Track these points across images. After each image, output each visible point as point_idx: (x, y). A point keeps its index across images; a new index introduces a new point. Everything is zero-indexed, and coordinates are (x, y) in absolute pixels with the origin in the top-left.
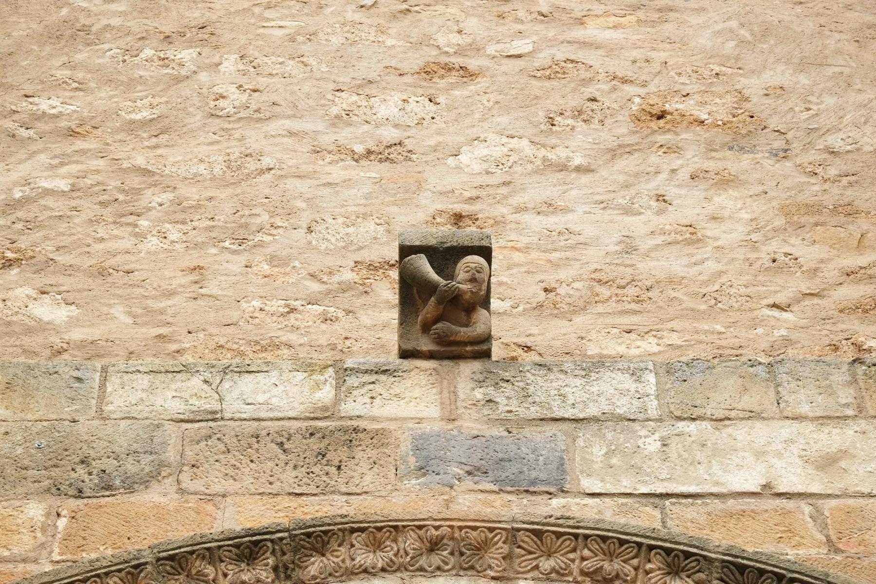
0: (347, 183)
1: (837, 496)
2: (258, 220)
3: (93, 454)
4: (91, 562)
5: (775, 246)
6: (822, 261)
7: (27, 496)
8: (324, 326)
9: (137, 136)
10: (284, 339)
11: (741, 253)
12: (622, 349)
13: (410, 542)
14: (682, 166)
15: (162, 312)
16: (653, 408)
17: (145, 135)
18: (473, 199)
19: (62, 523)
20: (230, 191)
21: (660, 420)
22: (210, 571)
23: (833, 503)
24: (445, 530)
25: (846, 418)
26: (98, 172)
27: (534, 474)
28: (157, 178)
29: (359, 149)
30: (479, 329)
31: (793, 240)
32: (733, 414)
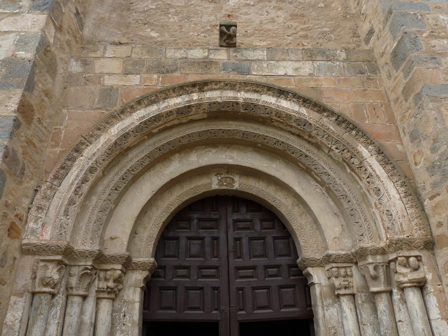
0: (208, 8)
2: (191, 15)
3: (165, 65)
4: (167, 87)
5: (289, 23)
6: (297, 26)
7: (154, 73)
8: (205, 38)
11: (282, 24)
12: (259, 44)
13: (222, 84)
14: (272, 5)
15: (175, 35)
16: (266, 59)
18: (232, 12)
19: (160, 79)
20: (186, 9)
21: (267, 60)
22: (187, 89)
23: (297, 77)
24: (228, 82)
25: (301, 60)
26: (160, 4)
27: (244, 71)
30: (234, 42)
31: (292, 22)
32: (280, 59)
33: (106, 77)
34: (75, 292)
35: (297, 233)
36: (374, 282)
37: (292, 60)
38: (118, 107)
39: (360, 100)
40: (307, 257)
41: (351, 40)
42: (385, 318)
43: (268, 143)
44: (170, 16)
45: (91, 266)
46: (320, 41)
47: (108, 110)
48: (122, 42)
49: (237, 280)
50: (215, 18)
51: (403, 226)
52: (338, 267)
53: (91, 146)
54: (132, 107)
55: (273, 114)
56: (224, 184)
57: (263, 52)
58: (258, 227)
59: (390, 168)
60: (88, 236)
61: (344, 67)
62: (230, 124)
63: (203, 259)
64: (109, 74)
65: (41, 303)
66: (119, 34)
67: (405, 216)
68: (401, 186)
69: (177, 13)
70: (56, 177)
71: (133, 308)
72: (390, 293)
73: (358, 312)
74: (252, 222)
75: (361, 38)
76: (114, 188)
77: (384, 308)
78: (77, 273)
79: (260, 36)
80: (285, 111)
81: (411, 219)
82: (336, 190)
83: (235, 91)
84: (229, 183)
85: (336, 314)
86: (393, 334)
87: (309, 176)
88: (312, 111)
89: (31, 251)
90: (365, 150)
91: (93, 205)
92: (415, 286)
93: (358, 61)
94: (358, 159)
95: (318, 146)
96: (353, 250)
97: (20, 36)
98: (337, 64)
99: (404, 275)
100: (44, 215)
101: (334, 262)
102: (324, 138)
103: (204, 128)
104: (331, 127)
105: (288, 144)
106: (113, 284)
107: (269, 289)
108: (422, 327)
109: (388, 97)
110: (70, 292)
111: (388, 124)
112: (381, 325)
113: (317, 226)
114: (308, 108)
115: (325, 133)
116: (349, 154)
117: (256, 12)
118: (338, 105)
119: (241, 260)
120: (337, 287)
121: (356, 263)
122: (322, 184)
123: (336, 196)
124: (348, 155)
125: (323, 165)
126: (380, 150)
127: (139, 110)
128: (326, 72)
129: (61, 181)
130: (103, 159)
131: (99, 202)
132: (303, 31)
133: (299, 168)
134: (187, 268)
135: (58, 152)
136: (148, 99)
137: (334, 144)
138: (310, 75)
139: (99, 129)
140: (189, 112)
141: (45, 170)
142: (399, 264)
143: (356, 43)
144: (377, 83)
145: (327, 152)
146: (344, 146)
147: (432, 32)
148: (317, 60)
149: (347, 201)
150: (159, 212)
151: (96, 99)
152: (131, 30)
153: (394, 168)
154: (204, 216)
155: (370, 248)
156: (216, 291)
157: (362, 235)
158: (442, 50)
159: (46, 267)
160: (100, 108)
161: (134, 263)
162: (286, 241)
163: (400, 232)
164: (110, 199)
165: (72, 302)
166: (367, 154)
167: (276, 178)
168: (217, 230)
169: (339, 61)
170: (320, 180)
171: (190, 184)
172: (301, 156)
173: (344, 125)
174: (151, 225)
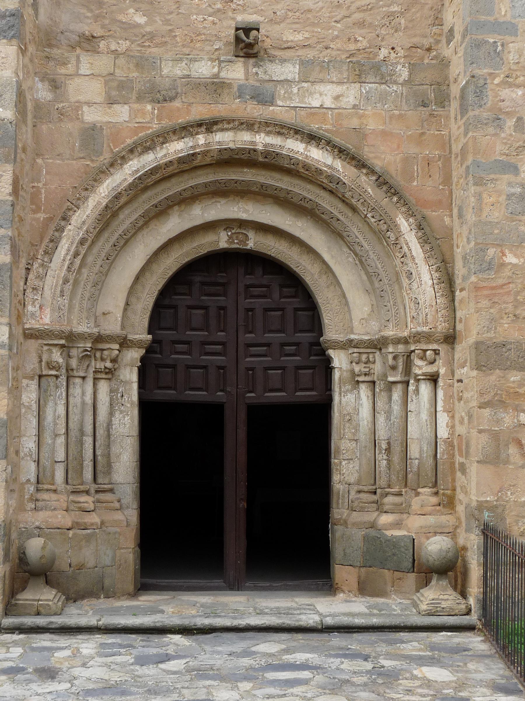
1: (338, 109)
6: (352, 3)
12: (292, 38)
13: (237, 123)
15: (169, 20)
16: (297, 79)
19: (156, 111)
22: (191, 129)
23: (336, 111)
24: (245, 121)
25: (344, 83)
30: (255, 51)
32: (317, 80)
33: (85, 108)
34: (75, 373)
35: (322, 308)
36: (392, 371)
37: (333, 82)
38: (106, 157)
39: (413, 150)
42: (396, 408)
43: (292, 198)
45: (91, 347)
47: (92, 161)
48: (95, 35)
49: (247, 359)
53: (79, 212)
54: (123, 158)
55: (300, 166)
56: (236, 241)
57: (295, 67)
58: (276, 295)
61: (402, 94)
62: (245, 172)
63: (206, 333)
64: (89, 104)
65: (49, 386)
66: (87, 17)
68: (436, 271)
70: (46, 253)
71: (131, 389)
72: (407, 383)
76: (105, 258)
77: (397, 398)
79: (294, 23)
80: (315, 164)
83: (253, 133)
84: (242, 241)
88: (348, 166)
90: (405, 222)
91: (84, 279)
92: (429, 379)
93: (423, 85)
94: (394, 234)
95: (354, 209)
98: (393, 90)
99: (420, 368)
100: (40, 296)
101: (355, 347)
102: (360, 203)
104: (369, 190)
107: (284, 369)
108: (426, 418)
109: (450, 146)
110: (71, 373)
111: (441, 187)
114: (344, 160)
116: (386, 226)
118: (383, 156)
119: (253, 335)
121: (380, 349)
124: (384, 227)
125: (357, 233)
127: (132, 160)
128: (375, 103)
130: (93, 227)
131: (90, 276)
132: (360, 11)
135: (42, 219)
136: (142, 145)
137: (370, 212)
138: (355, 107)
139: (86, 189)
140: (193, 160)
141: (30, 242)
143: (435, 37)
145: (363, 217)
146: (381, 215)
147: (507, 77)
148: (367, 81)
149: (378, 279)
150: (154, 278)
152: (105, 11)
156: (222, 371)
158: (510, 107)
159: (50, 352)
160: (83, 158)
161: (129, 340)
162: (310, 313)
163: (423, 323)
164: (102, 271)
165: (74, 383)
172: (332, 218)
173: (385, 188)
174: (146, 294)
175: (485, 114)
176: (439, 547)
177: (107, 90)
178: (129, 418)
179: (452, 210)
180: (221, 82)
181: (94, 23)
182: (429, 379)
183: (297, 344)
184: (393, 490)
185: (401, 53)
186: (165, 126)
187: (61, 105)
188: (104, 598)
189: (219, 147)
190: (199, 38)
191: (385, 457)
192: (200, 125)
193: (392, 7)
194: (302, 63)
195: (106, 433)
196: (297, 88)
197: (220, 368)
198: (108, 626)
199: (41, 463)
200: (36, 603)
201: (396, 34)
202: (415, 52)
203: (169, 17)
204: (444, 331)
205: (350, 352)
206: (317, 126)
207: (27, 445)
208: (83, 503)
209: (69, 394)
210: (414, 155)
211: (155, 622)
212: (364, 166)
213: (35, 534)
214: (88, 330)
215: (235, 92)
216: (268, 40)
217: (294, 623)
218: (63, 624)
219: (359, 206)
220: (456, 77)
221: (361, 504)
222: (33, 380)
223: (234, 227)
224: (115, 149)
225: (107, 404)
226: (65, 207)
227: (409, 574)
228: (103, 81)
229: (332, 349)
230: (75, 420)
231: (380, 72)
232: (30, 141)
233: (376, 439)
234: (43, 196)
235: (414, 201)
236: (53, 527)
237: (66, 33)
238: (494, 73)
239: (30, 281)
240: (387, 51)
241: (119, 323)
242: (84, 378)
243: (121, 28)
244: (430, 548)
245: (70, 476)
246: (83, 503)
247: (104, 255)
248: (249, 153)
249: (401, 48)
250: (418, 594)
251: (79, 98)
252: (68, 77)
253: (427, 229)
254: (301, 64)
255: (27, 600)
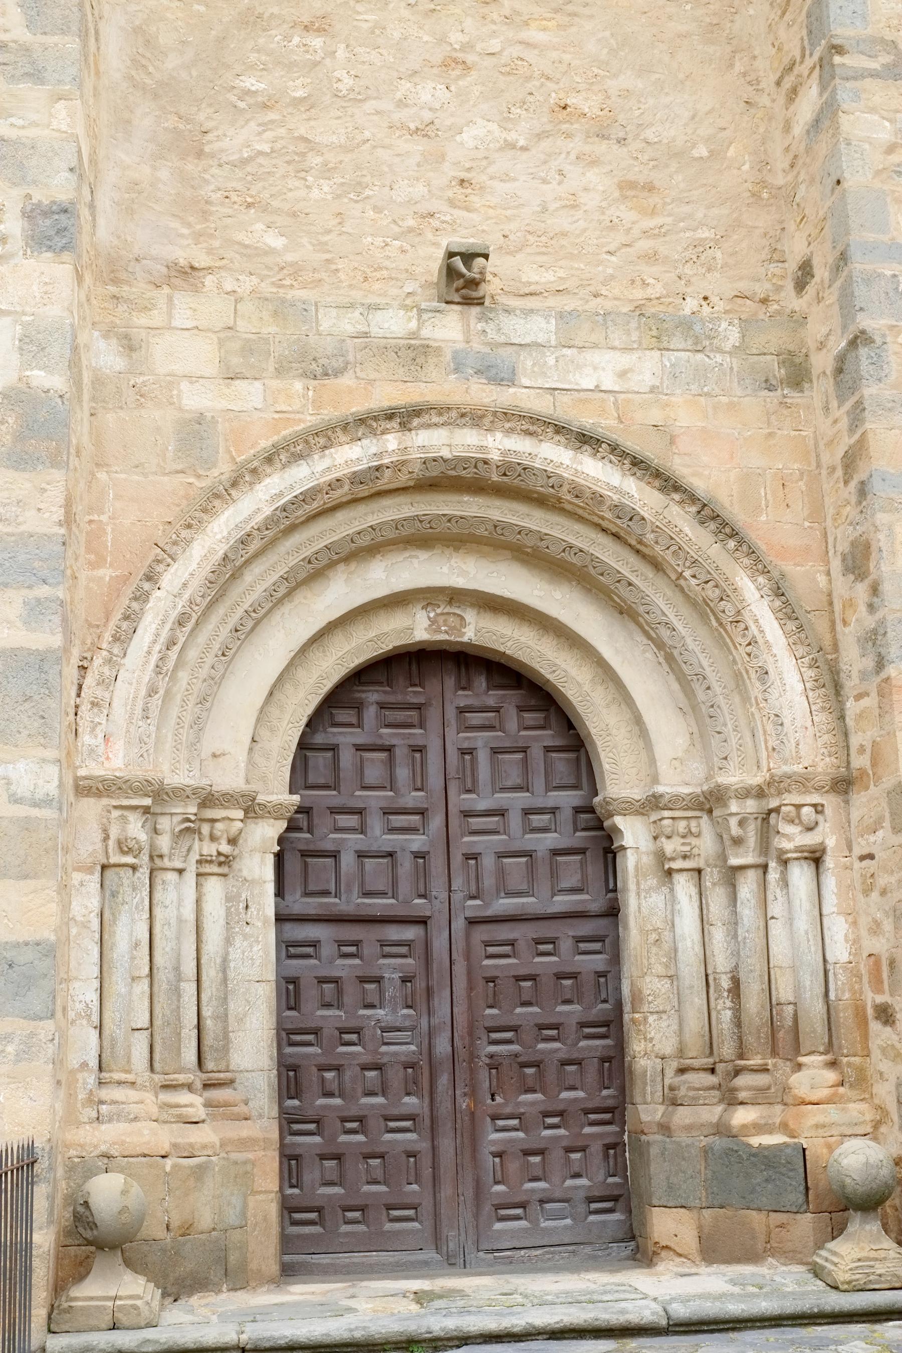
1: (625, 393)
3: (318, 356)
6: (633, 223)
9: (299, 110)
10: (384, 264)
12: (537, 278)
13: (454, 414)
14: (573, 148)
15: (326, 244)
17: (303, 109)
18: (469, 170)
19: (311, 393)
22: (374, 424)
23: (623, 396)
24: (468, 410)
25: (633, 349)
27: (502, 375)
28: (312, 144)
29: (412, 126)
30: (481, 294)
31: (622, 207)
32: (587, 345)
33: (184, 385)
34: (167, 863)
38: (223, 469)
40: (614, 796)
41: (763, 270)
42: (748, 912)
44: (310, 179)
46: (686, 271)
47: (199, 476)
50: (426, 189)
51: (800, 747)
52: (673, 818)
53: (176, 566)
54: (254, 471)
55: (565, 488)
58: (512, 724)
59: (794, 629)
60: (182, 756)
61: (731, 368)
62: (466, 502)
63: (391, 793)
66: (181, 236)
67: (806, 728)
68: (810, 667)
69: (329, 170)
70: (116, 639)
72: (765, 868)
73: (704, 902)
74: (498, 712)
75: (786, 265)
76: (220, 653)
77: (748, 895)
78: (168, 828)
80: (591, 486)
81: (818, 734)
82: (685, 663)
84: (454, 628)
85: (661, 905)
86: (756, 939)
87: (633, 624)
88: (648, 489)
89: (94, 790)
90: (750, 584)
92: (806, 858)
93: (765, 354)
95: (657, 565)
96: (705, 788)
97: (24, 325)
98: (716, 362)
99: (789, 838)
103: (407, 511)
104: (687, 530)
105: (592, 554)
106: (229, 847)
109: (818, 456)
110: (158, 863)
111: (807, 524)
112: (740, 925)
113: (641, 731)
115: (673, 542)
116: (717, 591)
117: (531, 171)
118: (706, 473)
120: (669, 856)
121: (710, 811)
122: (659, 644)
123: (684, 674)
124: (716, 594)
126: (779, 588)
128: (688, 384)
129: (125, 645)
130: (201, 594)
132: (648, 237)
133: (612, 603)
134: (360, 812)
135: (107, 579)
137: (689, 568)
138: (653, 390)
139: (189, 526)
140: (377, 478)
142: (783, 818)
144: (800, 416)
145: (674, 577)
148: (672, 347)
149: (704, 686)
151: (170, 448)
152: (213, 225)
153: (801, 628)
154: (391, 699)
155: (736, 787)
156: (421, 861)
157: (726, 758)
159: (123, 819)
165: (164, 881)
166: (753, 594)
167: (560, 622)
168: (421, 731)
169: (722, 352)
170: (654, 636)
171: (365, 629)
172: (619, 581)
173: (713, 526)
174: (286, 722)
175: (888, 392)
176: (862, 1159)
177: (222, 355)
178: (260, 947)
179: (829, 562)
180: (423, 346)
181: (193, 246)
182: (806, 858)
183: (553, 811)
184: (751, 1062)
185: (719, 306)
186: (327, 418)
187: (140, 380)
188: (229, 1290)
189: (422, 456)
190: (378, 275)
191: (729, 1004)
192: (390, 417)
193: (700, 231)
194: (561, 316)
195: (220, 975)
196: (553, 356)
197: (418, 855)
198: (259, 1343)
199: (106, 1032)
200: (110, 1304)
201: (707, 275)
202: (740, 305)
203: (326, 238)
204: (829, 770)
205: (653, 818)
206: (591, 421)
207: (81, 997)
208: (186, 1106)
209: (154, 902)
210: (759, 471)
211: (351, 1330)
212: (677, 488)
213: (98, 1167)
214: (192, 782)
215: (448, 364)
216: (496, 281)
217: (615, 1317)
218: (171, 1343)
219: (668, 556)
220: (822, 339)
221: (691, 1093)
222: (92, 873)
223: (440, 603)
224: (239, 456)
225: (222, 922)
226: (151, 558)
227: (799, 1216)
228: (216, 340)
229: (620, 814)
230: (167, 949)
231: (692, 333)
232: (85, 439)
233: (709, 972)
234: (109, 538)
235: (764, 547)
236: (133, 1153)
237: (144, 262)
238: (897, 326)
239: (86, 691)
240: (695, 302)
241: (242, 774)
242: (181, 871)
243: (241, 254)
244: (845, 1162)
245: (157, 1056)
246: (186, 1106)
247: (218, 646)
248: (476, 467)
249: (718, 298)
250: (823, 1253)
251: (173, 367)
252: (152, 332)
253: (790, 595)
254: (558, 316)
255: (92, 1299)
